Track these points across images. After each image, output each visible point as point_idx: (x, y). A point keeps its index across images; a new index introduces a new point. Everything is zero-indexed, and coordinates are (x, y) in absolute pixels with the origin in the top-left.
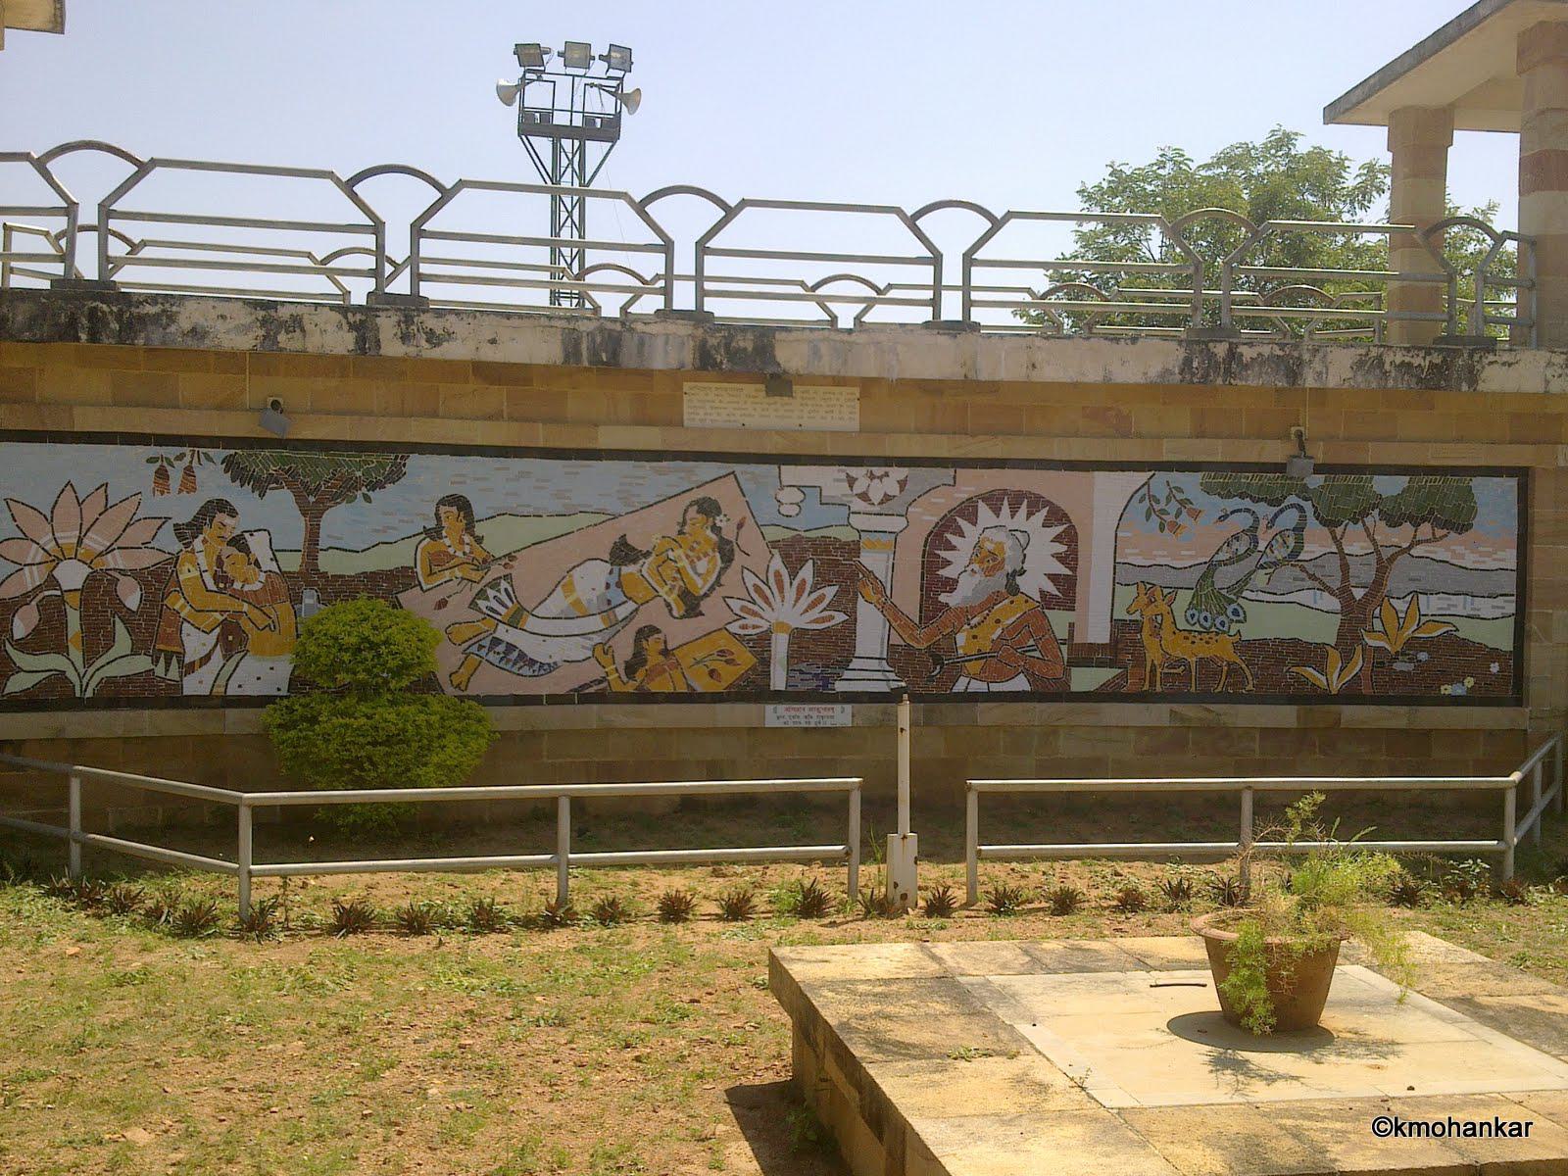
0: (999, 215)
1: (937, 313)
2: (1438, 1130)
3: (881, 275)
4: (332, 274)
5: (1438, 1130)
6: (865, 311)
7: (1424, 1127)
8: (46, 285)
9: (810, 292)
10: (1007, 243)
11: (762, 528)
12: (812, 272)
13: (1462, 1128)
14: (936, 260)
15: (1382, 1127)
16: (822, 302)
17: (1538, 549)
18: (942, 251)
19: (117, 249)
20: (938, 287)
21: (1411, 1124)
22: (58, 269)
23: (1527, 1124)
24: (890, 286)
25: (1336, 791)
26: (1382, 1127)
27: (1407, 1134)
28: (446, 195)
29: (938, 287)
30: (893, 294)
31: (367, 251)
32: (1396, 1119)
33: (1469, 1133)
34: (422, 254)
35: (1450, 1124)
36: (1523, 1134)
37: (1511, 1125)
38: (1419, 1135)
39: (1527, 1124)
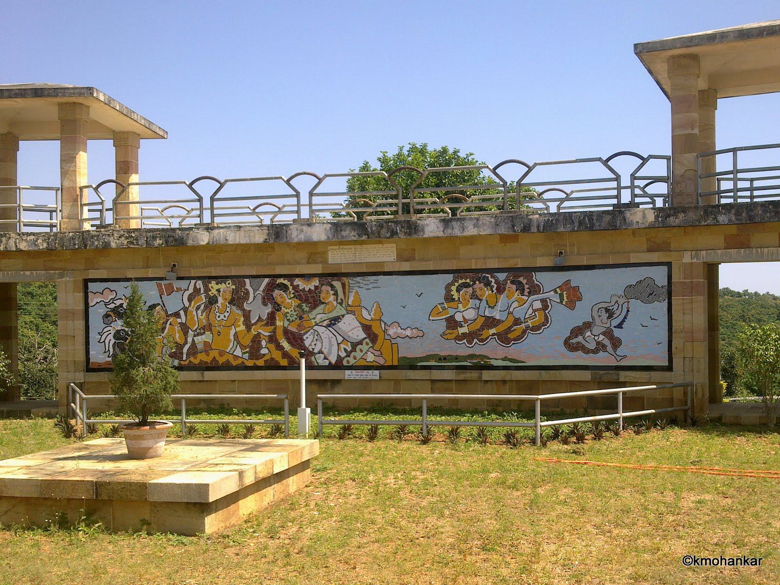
0: (531, 165)
1: (619, 201)
2: (716, 562)
3: (280, 202)
4: (545, 201)
5: (716, 562)
6: (274, 217)
7: (708, 561)
8: (611, 208)
9: (254, 212)
10: (327, 186)
11: (544, 292)
12: (252, 204)
13: (727, 562)
14: (297, 195)
15: (688, 561)
16: (167, 218)
17: (81, 307)
18: (202, 196)
19: (637, 191)
20: (299, 205)
21: (702, 559)
22: (615, 201)
23: (760, 559)
24: (284, 206)
25: (490, 400)
26: (688, 561)
27: (700, 564)
28: (320, 180)
29: (299, 205)
30: (285, 209)
31: (614, 189)
32: (695, 557)
33: (731, 563)
34: (732, 182)
35: (721, 559)
36: (758, 563)
37: (729, 560)
38: (706, 565)
39: (760, 559)
